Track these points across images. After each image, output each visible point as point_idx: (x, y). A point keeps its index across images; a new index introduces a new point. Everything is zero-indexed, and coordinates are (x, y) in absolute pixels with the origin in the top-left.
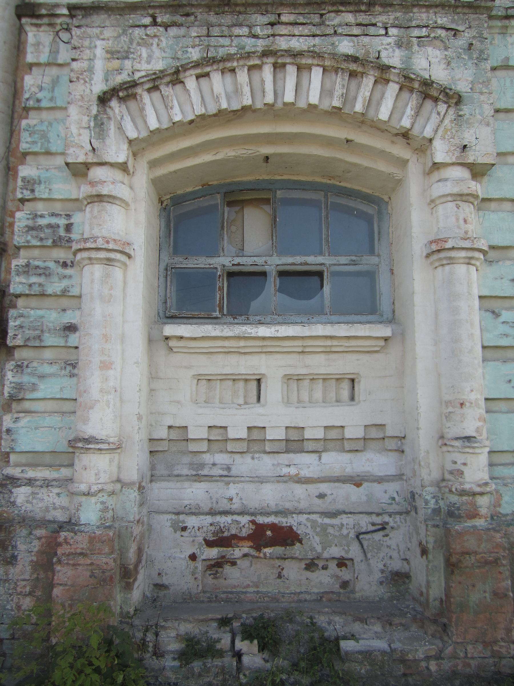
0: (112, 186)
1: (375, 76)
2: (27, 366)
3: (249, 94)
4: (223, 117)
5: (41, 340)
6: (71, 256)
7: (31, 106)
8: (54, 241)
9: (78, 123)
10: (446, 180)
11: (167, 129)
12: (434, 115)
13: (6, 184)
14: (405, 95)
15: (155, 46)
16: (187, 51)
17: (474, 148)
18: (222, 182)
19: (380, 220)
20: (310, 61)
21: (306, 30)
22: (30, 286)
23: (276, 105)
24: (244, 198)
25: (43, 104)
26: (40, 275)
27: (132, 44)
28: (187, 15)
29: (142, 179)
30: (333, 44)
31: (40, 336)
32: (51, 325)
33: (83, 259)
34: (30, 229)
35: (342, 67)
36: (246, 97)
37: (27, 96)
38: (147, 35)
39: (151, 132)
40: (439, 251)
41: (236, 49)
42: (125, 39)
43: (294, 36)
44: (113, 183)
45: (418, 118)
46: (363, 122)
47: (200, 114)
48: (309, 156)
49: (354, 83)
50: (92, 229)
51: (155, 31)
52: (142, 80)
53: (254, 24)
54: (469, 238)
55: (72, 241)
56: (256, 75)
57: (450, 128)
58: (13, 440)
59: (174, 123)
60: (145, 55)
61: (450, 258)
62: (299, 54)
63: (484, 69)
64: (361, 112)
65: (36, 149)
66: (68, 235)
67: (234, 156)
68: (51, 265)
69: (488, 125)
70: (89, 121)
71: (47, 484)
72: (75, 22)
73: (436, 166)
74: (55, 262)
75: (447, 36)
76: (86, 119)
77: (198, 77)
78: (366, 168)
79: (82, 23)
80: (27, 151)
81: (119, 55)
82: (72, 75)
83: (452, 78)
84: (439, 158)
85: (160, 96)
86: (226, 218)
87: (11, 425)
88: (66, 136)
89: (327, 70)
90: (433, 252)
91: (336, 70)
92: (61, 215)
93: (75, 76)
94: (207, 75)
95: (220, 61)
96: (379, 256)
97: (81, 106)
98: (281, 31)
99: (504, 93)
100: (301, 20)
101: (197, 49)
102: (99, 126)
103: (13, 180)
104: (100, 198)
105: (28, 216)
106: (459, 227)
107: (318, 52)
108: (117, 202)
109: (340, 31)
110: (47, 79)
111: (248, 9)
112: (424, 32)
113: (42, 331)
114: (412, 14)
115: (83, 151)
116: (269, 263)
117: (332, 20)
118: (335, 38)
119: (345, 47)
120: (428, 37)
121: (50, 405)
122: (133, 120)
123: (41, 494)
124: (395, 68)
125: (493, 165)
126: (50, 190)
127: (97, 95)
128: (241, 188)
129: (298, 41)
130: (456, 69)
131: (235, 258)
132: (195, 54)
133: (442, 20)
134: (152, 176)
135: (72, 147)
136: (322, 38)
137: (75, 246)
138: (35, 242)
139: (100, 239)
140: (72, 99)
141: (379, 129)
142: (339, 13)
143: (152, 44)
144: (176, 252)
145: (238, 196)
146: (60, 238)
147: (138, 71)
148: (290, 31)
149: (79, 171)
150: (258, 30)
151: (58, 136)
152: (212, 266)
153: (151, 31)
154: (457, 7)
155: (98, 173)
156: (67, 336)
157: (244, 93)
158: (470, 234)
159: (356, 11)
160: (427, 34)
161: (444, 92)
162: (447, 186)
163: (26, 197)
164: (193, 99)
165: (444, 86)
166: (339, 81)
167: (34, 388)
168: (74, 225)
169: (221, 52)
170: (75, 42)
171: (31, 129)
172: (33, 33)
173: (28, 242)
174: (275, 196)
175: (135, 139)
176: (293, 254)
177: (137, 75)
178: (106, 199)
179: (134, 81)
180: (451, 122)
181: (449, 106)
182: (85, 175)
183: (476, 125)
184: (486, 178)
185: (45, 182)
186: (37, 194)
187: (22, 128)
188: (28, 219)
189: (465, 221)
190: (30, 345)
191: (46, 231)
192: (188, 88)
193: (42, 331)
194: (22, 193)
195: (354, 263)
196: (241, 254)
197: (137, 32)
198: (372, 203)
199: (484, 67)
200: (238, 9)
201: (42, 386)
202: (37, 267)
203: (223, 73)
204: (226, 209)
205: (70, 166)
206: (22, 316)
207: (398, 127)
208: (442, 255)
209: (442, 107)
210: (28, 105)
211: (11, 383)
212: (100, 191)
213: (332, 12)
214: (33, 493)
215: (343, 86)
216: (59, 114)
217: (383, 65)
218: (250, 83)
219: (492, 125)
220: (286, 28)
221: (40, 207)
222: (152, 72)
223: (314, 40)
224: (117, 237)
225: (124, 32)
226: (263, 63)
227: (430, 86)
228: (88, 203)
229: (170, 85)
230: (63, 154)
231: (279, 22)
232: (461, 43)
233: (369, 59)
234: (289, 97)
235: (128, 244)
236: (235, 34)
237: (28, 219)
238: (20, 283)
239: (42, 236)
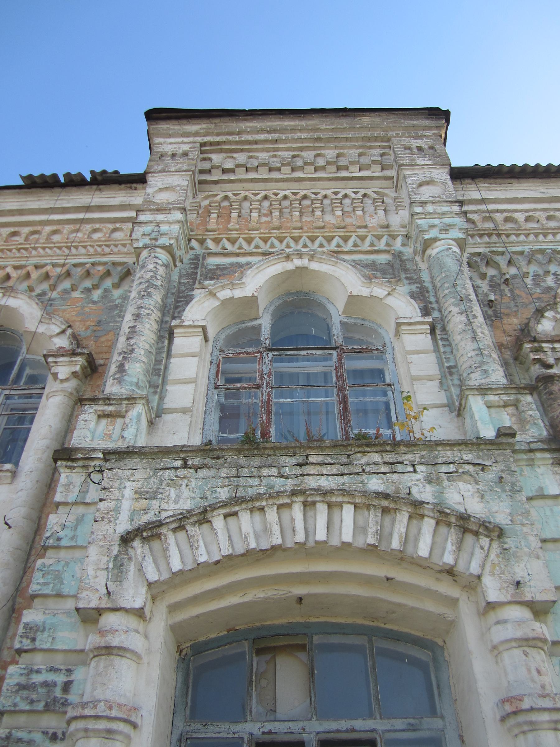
0: (124, 636)
1: (409, 512)
3: (279, 533)
4: (252, 557)
6: (64, 725)
7: (50, 545)
8: (47, 705)
9: (96, 564)
10: (505, 622)
11: (190, 570)
12: (478, 550)
13: (6, 629)
14: (443, 529)
15: (184, 486)
16: (216, 492)
17: (528, 583)
18: (251, 626)
19: (437, 669)
20: (340, 499)
21: (334, 470)
23: (308, 543)
24: (275, 644)
25: (63, 543)
27: (161, 485)
28: (218, 458)
29: (159, 626)
30: (362, 482)
33: (77, 730)
34: (22, 687)
35: (374, 503)
36: (275, 536)
37: (48, 534)
38: (176, 476)
39: (173, 573)
40: (515, 713)
41: (265, 488)
42: (155, 480)
43: (323, 475)
44: (126, 632)
45: (461, 553)
46: (402, 559)
47: (227, 554)
48: (347, 596)
49: (387, 520)
50: (94, 689)
51: (185, 472)
52: (168, 520)
53: (283, 465)
54: (548, 695)
55: (69, 704)
56: (285, 514)
57: (497, 562)
59: (198, 564)
61: (531, 723)
62: (330, 492)
63: (519, 501)
64: (398, 548)
65: (47, 590)
66: (64, 696)
67: (263, 598)
68: (37, 737)
69: (538, 558)
70: (109, 562)
72: (108, 465)
73: (491, 606)
74: (43, 733)
75: (475, 470)
77: (226, 516)
78: (412, 608)
79: (114, 466)
80: (37, 593)
81: (147, 496)
82: (98, 514)
83: (489, 511)
84: (493, 596)
85: (186, 535)
86: (254, 670)
88: (81, 578)
89: (359, 507)
90: (508, 715)
91: (368, 507)
92: (61, 670)
93: (101, 515)
94: (235, 514)
95: (249, 500)
96: (442, 717)
97: (102, 546)
98: (310, 471)
99: (547, 522)
100: (329, 460)
101: (226, 489)
102: (118, 568)
103: (15, 623)
104: (108, 650)
105: (23, 671)
106: (533, 681)
107: (347, 489)
108: (128, 655)
109: (368, 469)
110: (72, 518)
111: (277, 452)
112: (452, 468)
114: (437, 452)
115: (98, 595)
116: (307, 730)
117: (359, 460)
118: (364, 477)
119: (375, 484)
120: (456, 472)
122: (155, 561)
124: (427, 503)
125: (555, 602)
126: (53, 638)
127: (120, 535)
128: (272, 634)
129: (327, 480)
130: (491, 501)
131: (265, 724)
132: (224, 494)
133: (468, 456)
134: (170, 622)
136: (351, 476)
137: (71, 713)
138: (24, 706)
139: (102, 703)
140: (93, 539)
141: (420, 566)
142: (366, 454)
143: (181, 485)
144: (194, 714)
145: (267, 641)
146: (55, 700)
147: (165, 510)
148: (318, 471)
149: (90, 617)
150: (287, 471)
151: (73, 576)
152: (236, 736)
153: (182, 472)
154: (480, 444)
155: (110, 620)
157: (274, 532)
158: (548, 690)
159: (382, 451)
160: (455, 469)
161: (484, 525)
162: (507, 629)
163: (25, 648)
164: (220, 538)
165: (482, 520)
166: (372, 519)
168: (75, 683)
169: (251, 492)
170: (105, 483)
171: (46, 569)
172: (66, 474)
173: (15, 705)
174: (312, 643)
175: (156, 581)
176: (337, 718)
177: (164, 515)
179: (160, 521)
180: (498, 556)
181: (492, 540)
182: (96, 621)
183: (525, 558)
184: (550, 617)
185: (50, 629)
186: (38, 644)
187: (36, 567)
189: (539, 672)
191: (40, 690)
192: (215, 527)
195: (412, 728)
196: (272, 718)
197: (167, 474)
198: (425, 648)
199: (519, 498)
200: (266, 452)
203: (251, 511)
204: (255, 659)
205: (80, 611)
207: (441, 564)
208: (521, 718)
209: (485, 541)
210: (47, 544)
212: (110, 641)
213: (359, 452)
215: (377, 522)
216: (78, 554)
217: (416, 501)
218: (280, 522)
219: (543, 558)
220: (315, 468)
221: (38, 660)
222: (179, 512)
223: (343, 478)
224: (123, 701)
225: (155, 474)
226: (292, 502)
227: (468, 519)
228: (94, 657)
229: (197, 525)
230: (75, 596)
231: (307, 463)
232: (490, 476)
233: (401, 496)
234: (321, 535)
235: (135, 709)
236: (264, 474)
237: (21, 675)
239: (34, 697)
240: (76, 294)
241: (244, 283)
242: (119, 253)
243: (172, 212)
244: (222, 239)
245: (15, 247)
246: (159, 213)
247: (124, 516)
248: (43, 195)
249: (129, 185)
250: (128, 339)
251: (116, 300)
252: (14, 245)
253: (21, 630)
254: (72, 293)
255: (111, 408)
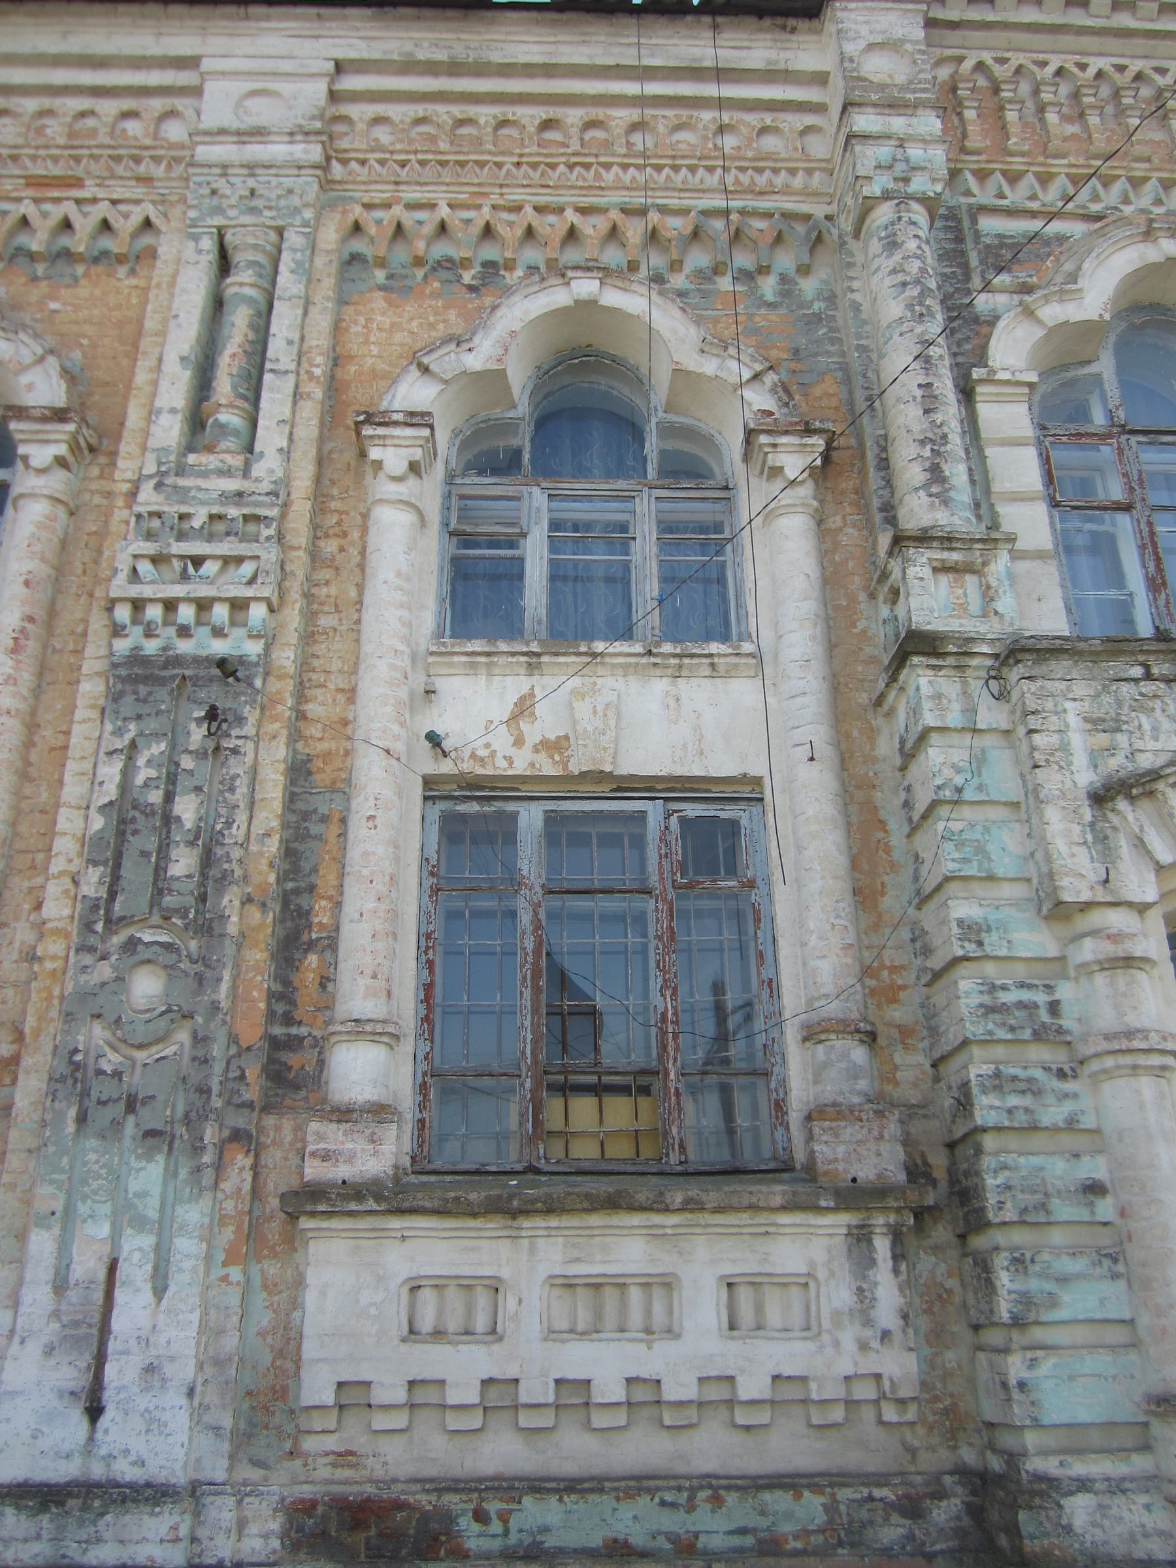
2: (1033, 1261)
5: (1048, 1212)
15: (1158, 712)
22: (1010, 1111)
26: (1023, 1092)
31: (1044, 1205)
32: (1058, 1182)
34: (989, 1010)
38: (1141, 694)
58: (1033, 1403)
60: (1146, 726)
68: (1038, 1074)
70: (1084, 832)
71: (1118, 1487)
74: (1044, 1068)
76: (1077, 829)
79: (1033, 673)
87: (1025, 1374)
93: (1043, 757)
113: (1046, 1194)
121: (1080, 1334)
123: (1115, 1509)
135: (1066, 875)
138: (1002, 1034)
143: (1153, 710)
153: (1148, 687)
156: (1092, 1204)
167: (1053, 1302)
173: (990, 1033)
178: (1136, 964)
186: (988, 949)
188: (981, 992)
190: (1029, 1219)
191: (1017, 1013)
193: (1046, 1194)
194: (963, 947)
201: (1066, 1297)
202: (1015, 1078)
206: (1005, 1167)
211: (1009, 1292)
214: (1101, 1506)
237: (981, 992)
238: (992, 1107)
239: (1013, 1022)
240: (725, 283)
241: (1080, 290)
242: (786, 191)
243: (920, 112)
244: (992, 171)
245: (563, 159)
246: (892, 111)
247: (1080, 760)
248: (590, 30)
249: (780, 21)
250: (927, 412)
251: (812, 302)
252: (562, 155)
253: (956, 930)
254: (718, 279)
255: (955, 556)
